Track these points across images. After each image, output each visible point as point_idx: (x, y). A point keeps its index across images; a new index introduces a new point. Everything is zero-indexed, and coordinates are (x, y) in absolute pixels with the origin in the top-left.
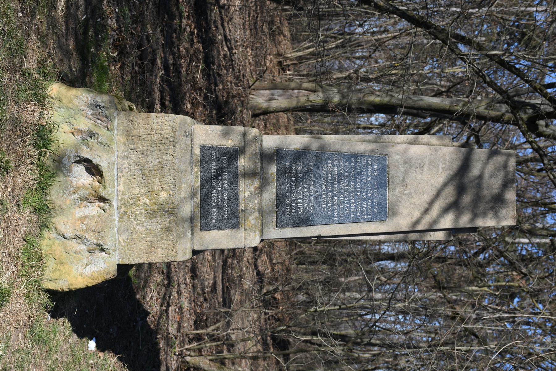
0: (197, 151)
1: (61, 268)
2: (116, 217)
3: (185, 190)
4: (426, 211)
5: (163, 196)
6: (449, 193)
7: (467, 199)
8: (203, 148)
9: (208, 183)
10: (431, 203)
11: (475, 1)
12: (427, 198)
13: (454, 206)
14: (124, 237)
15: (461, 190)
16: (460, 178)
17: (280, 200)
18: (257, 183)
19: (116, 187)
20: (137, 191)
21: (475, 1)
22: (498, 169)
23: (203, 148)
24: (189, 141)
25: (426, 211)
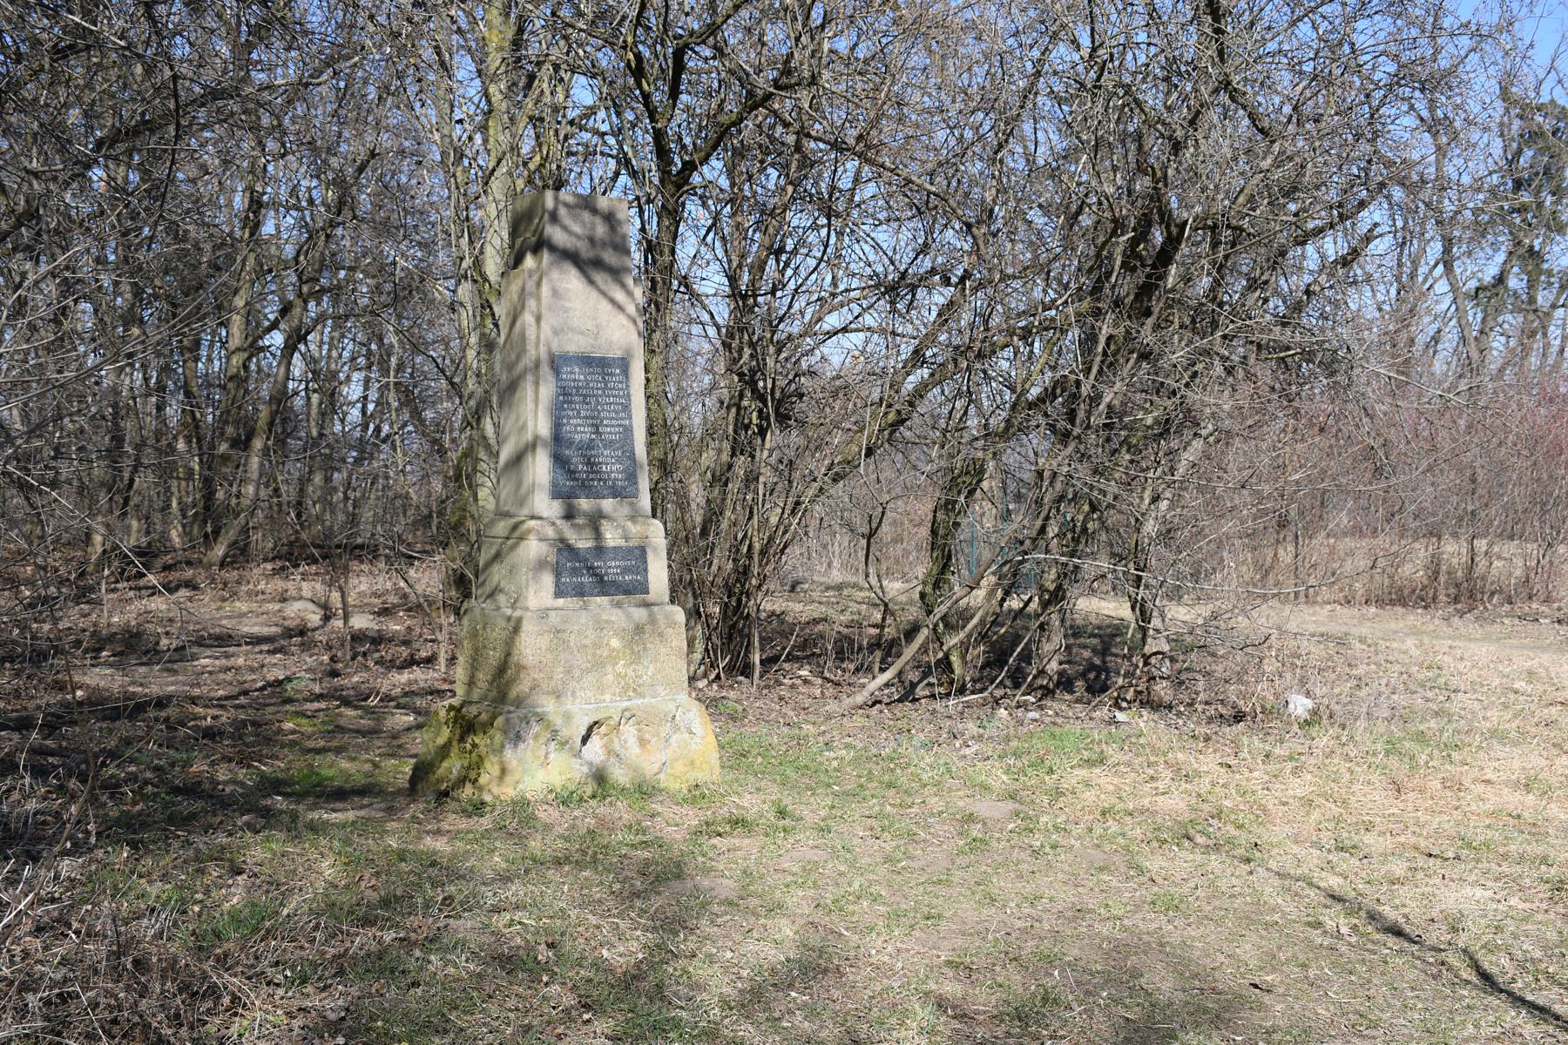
0: (561, 602)
1: (697, 763)
2: (639, 702)
3: (615, 616)
4: (620, 308)
5: (615, 643)
6: (600, 278)
7: (609, 257)
8: (559, 594)
9: (604, 586)
10: (612, 301)
11: (91, 1036)
12: (605, 305)
13: (616, 273)
14: (660, 689)
15: (598, 264)
16: (587, 264)
17: (616, 493)
18: (604, 522)
19: (611, 705)
20: (610, 677)
21: (91, 1036)
22: (576, 218)
23: (559, 594)
24: (552, 614)
25: (620, 308)
